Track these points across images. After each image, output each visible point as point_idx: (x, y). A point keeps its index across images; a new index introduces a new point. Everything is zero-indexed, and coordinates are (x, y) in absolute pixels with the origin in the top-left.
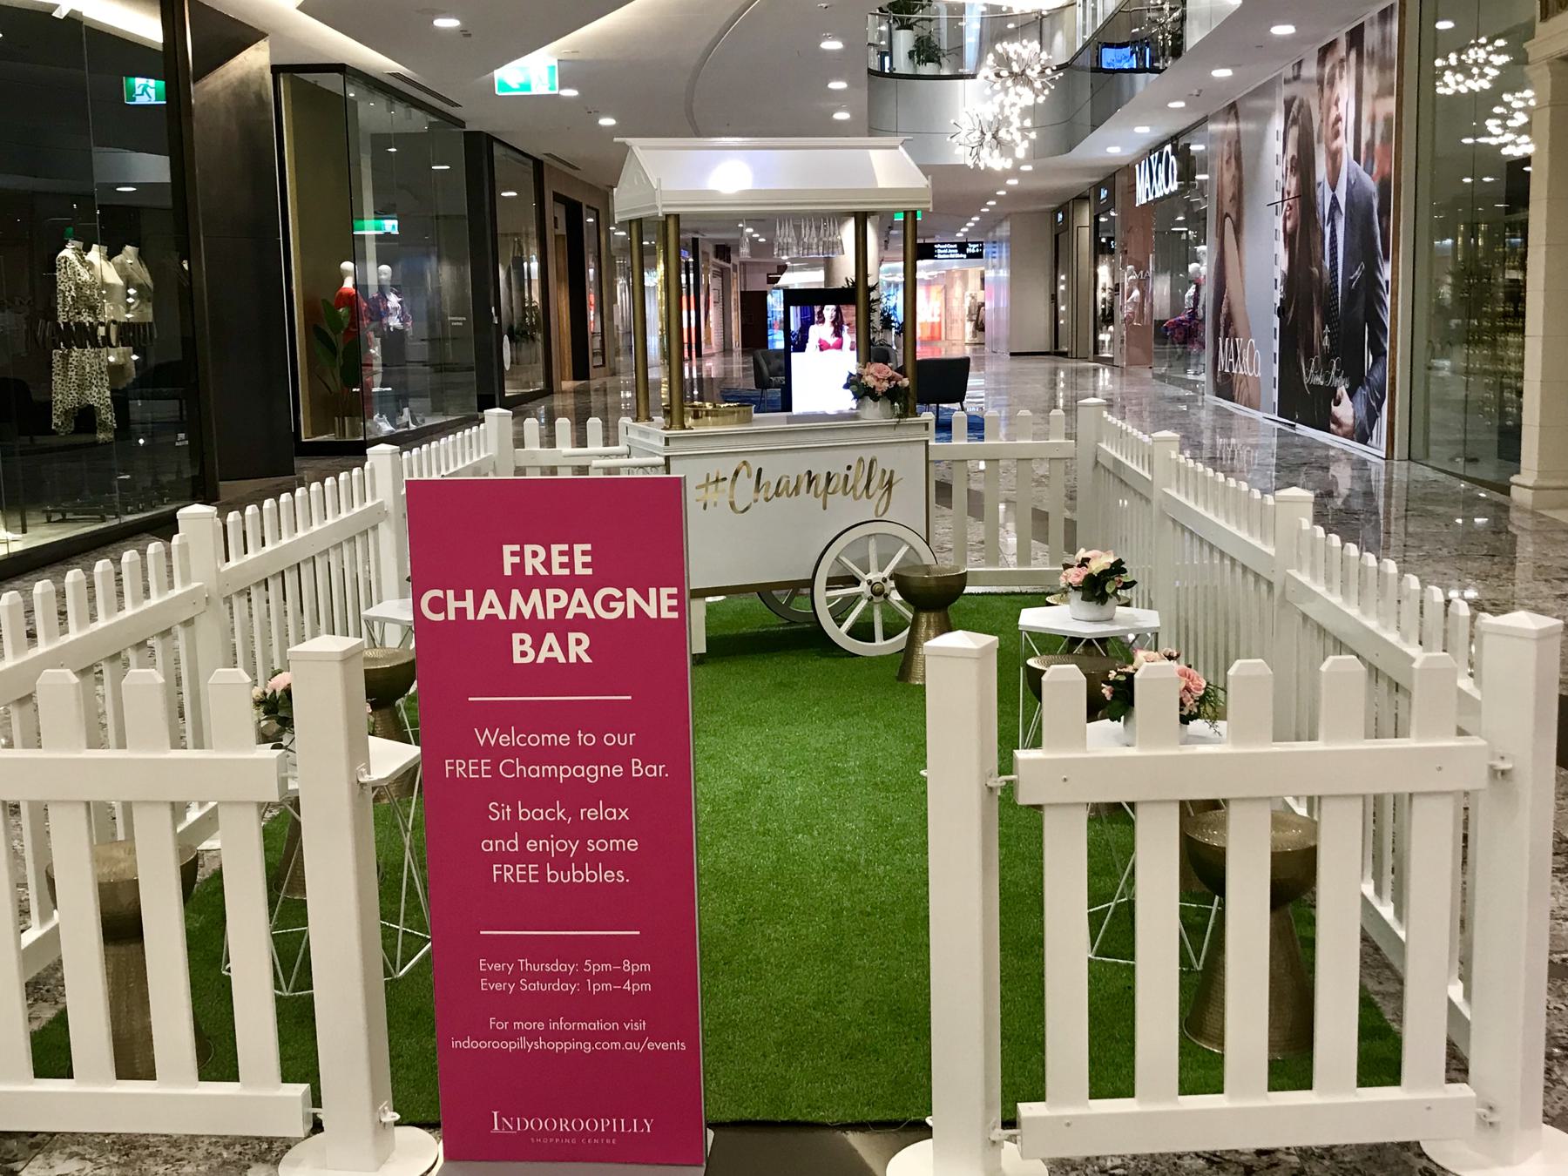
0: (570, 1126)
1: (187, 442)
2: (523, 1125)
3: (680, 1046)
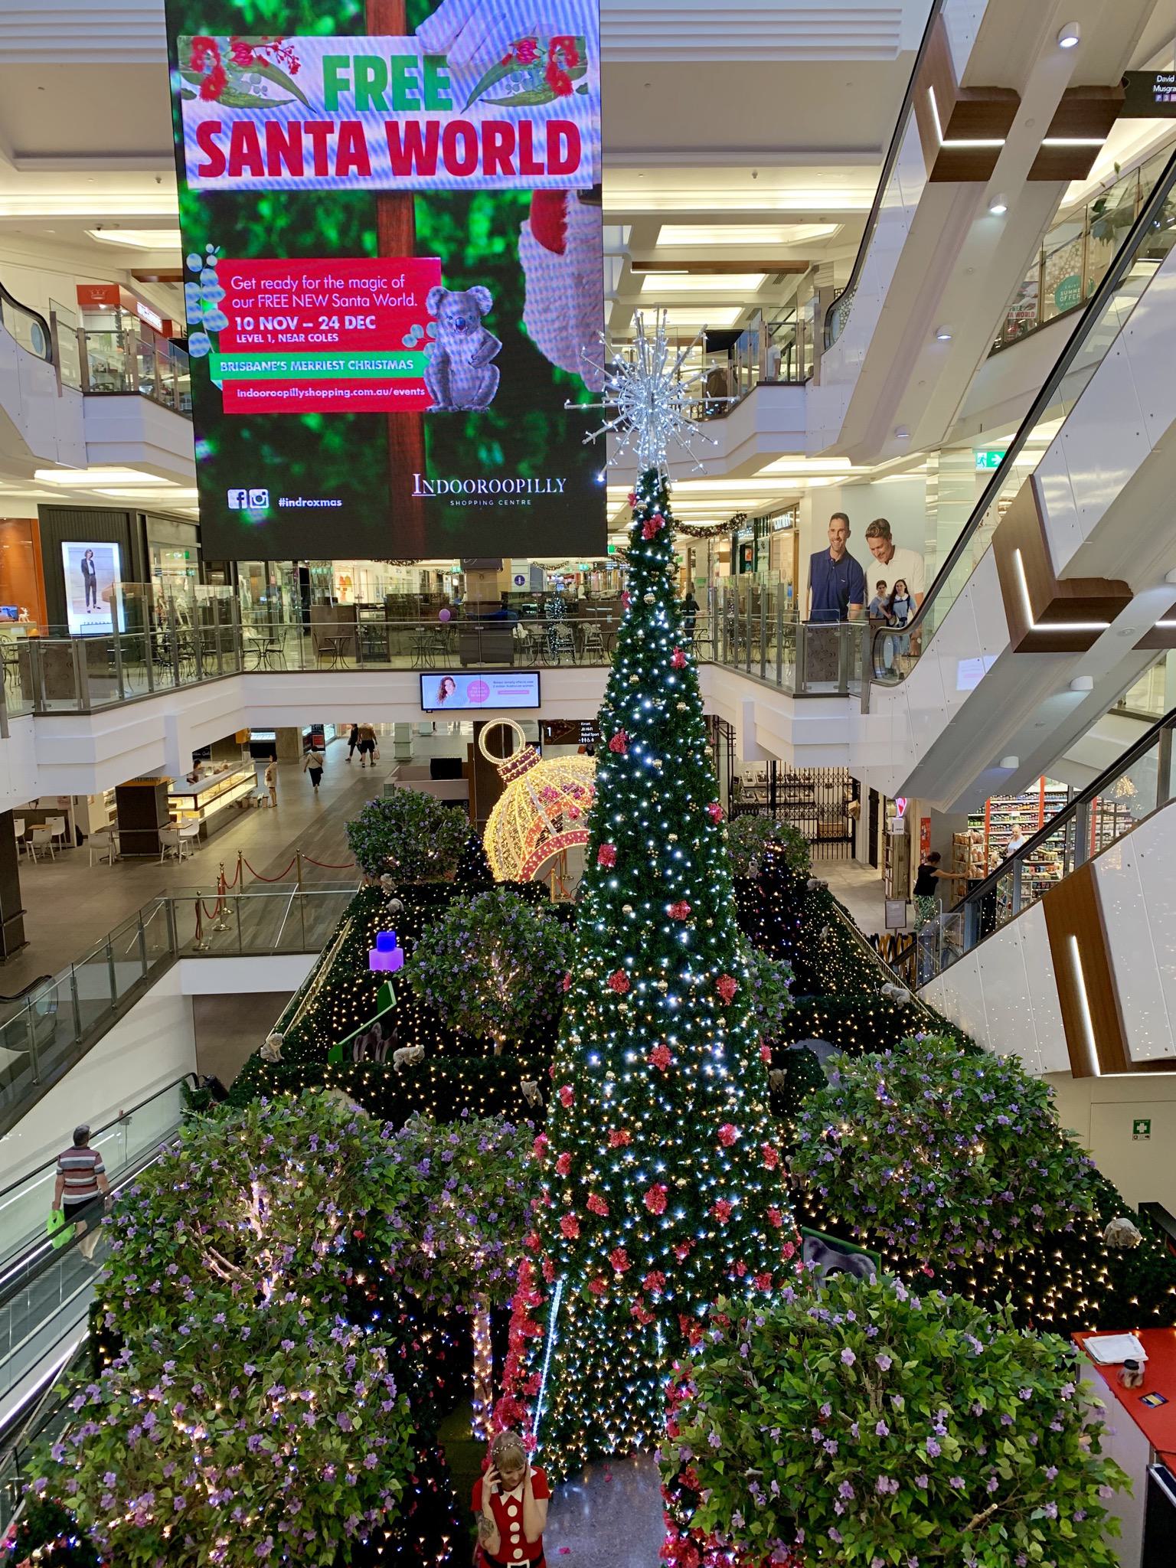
0: (487, 487)
1: (527, 1562)
2: (443, 486)
3: (282, 502)
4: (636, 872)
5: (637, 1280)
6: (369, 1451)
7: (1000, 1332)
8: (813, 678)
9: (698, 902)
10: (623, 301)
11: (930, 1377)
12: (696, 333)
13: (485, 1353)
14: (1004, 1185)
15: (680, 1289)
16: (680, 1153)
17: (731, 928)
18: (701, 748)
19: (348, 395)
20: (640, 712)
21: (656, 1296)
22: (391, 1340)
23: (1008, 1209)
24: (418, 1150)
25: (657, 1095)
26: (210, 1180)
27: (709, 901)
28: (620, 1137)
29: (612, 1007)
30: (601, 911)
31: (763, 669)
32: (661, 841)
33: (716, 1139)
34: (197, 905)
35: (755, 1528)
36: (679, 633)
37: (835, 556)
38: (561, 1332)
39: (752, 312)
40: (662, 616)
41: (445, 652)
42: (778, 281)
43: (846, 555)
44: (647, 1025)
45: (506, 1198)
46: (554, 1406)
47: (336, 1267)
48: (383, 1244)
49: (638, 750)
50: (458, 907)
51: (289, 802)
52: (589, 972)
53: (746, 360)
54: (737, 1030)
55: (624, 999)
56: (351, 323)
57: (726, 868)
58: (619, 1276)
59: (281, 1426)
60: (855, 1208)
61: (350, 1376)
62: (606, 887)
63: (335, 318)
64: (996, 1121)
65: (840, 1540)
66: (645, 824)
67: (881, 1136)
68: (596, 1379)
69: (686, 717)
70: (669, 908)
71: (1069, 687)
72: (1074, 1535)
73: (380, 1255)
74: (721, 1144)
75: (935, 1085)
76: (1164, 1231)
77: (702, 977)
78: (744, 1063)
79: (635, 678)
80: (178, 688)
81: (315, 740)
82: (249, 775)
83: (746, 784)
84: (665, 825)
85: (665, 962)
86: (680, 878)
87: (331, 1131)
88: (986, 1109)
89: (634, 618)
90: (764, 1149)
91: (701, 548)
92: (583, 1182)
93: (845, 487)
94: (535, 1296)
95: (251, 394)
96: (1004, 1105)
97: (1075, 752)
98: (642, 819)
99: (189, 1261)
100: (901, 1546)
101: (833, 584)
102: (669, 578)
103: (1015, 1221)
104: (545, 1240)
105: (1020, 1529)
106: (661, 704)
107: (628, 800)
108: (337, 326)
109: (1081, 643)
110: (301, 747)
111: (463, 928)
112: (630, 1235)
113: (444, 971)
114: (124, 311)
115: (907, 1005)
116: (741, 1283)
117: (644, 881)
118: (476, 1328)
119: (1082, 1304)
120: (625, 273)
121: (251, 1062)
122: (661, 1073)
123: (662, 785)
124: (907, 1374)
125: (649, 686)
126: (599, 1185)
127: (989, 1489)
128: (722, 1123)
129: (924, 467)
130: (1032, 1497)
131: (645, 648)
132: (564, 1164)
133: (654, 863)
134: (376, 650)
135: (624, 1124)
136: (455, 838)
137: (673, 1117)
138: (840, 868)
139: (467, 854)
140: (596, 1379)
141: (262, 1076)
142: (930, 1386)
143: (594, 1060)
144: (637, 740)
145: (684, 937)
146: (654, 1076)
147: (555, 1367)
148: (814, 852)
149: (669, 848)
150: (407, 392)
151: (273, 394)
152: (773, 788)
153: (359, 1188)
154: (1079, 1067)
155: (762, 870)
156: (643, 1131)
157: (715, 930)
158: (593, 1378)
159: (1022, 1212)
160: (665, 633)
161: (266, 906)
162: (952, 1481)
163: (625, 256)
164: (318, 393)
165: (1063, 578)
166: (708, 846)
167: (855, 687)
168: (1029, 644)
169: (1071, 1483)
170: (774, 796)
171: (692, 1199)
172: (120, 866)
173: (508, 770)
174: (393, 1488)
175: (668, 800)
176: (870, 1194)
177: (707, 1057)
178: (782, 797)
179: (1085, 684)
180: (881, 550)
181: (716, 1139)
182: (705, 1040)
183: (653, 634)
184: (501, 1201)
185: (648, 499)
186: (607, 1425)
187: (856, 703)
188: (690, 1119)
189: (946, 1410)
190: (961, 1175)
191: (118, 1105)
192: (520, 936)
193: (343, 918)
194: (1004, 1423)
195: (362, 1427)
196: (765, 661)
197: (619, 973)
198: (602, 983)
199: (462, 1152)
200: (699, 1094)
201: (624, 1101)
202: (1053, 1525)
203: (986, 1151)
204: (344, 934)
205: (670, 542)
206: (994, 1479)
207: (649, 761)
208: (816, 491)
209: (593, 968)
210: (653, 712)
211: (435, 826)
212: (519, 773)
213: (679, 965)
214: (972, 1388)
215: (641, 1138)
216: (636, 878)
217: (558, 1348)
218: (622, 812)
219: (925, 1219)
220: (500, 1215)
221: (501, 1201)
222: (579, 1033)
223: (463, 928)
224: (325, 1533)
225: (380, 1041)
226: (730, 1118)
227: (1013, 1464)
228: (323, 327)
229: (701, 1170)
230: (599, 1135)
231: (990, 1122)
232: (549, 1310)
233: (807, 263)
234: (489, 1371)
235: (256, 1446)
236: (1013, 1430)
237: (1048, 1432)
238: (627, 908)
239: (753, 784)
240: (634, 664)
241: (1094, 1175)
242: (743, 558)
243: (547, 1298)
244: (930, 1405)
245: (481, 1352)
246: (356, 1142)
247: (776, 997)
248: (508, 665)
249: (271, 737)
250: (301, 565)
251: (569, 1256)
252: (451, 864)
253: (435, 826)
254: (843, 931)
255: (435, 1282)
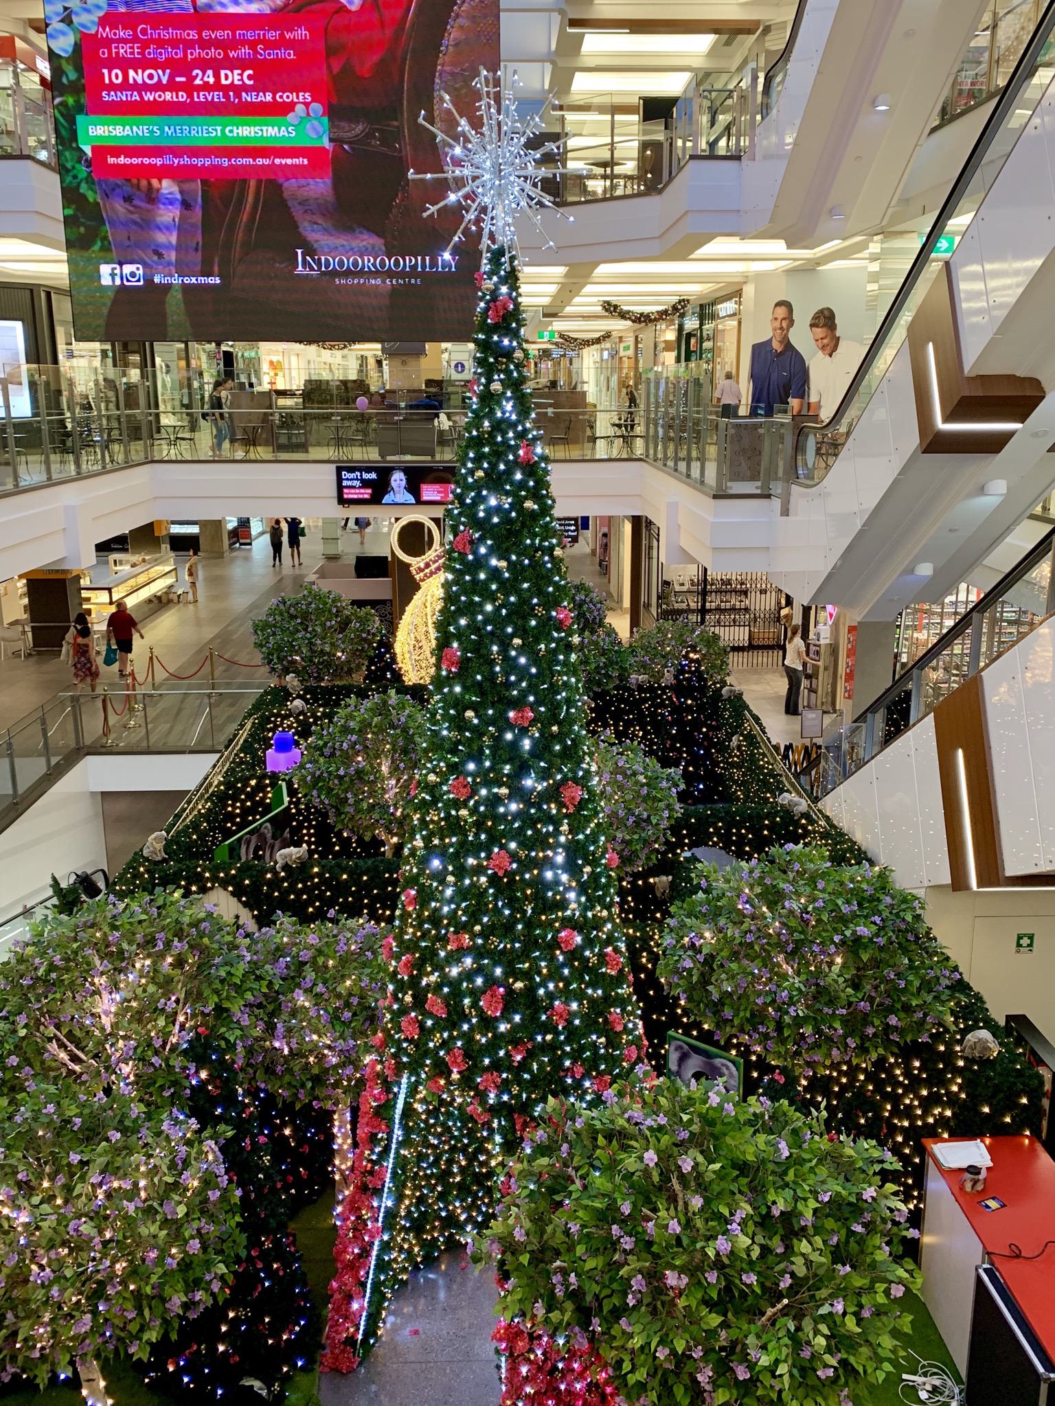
4: (479, 677)
5: (473, 1080)
6: (192, 1237)
7: (817, 1138)
8: (737, 477)
9: (542, 709)
10: (561, 63)
11: (735, 1179)
12: (635, 100)
13: (345, 1147)
14: (860, 995)
15: (515, 1090)
16: (518, 957)
17: (578, 735)
18: (551, 549)
19: (226, 164)
20: (485, 511)
21: (492, 1095)
22: (230, 1134)
23: (866, 1020)
24: (277, 949)
25: (496, 899)
26: (54, 975)
27: (554, 708)
28: (458, 940)
29: (453, 813)
30: (446, 716)
31: (676, 464)
32: (505, 646)
33: (555, 944)
34: (104, 701)
35: (555, 1316)
36: (528, 425)
37: (777, 346)
38: (407, 1130)
39: (702, 78)
40: (509, 406)
41: (365, 443)
42: (728, 43)
43: (788, 346)
44: (489, 832)
45: (361, 998)
46: (400, 1198)
47: (177, 1062)
48: (227, 1041)
49: (483, 550)
50: (349, 709)
51: (214, 598)
52: (432, 778)
53: (680, 132)
54: (581, 837)
55: (465, 804)
56: (227, 77)
57: (575, 674)
58: (455, 1076)
59: (102, 1213)
60: (714, 1014)
61: (180, 1167)
62: (451, 691)
63: (210, 72)
64: (854, 932)
65: (629, 1330)
66: (489, 628)
67: (740, 944)
68: (453, 1175)
69: (534, 516)
70: (511, 714)
71: (981, 490)
72: (860, 1330)
73: (224, 1052)
74: (560, 948)
75: (798, 895)
76: (1027, 1043)
77: (545, 784)
78: (588, 869)
79: (480, 474)
80: (80, 476)
81: (241, 533)
82: (168, 569)
83: (678, 588)
84: (510, 630)
85: (507, 768)
86: (524, 684)
87: (181, 929)
88: (844, 920)
89: (481, 409)
90: (606, 954)
91: (647, 335)
92: (424, 983)
93: (790, 272)
94: (380, 1093)
95: (122, 160)
96: (866, 917)
97: (991, 560)
98: (486, 622)
99: (31, 1053)
100: (687, 1336)
101: (774, 377)
102: (517, 366)
103: (870, 1031)
104: (388, 1039)
105: (807, 1324)
106: (507, 502)
107: (472, 602)
108: (212, 80)
109: (994, 444)
110: (226, 542)
111: (352, 732)
112: (468, 1038)
113: (330, 773)
114: (22, 66)
115: (806, 815)
116: (578, 1084)
117: (487, 685)
118: (336, 1123)
119: (936, 1112)
120: (562, 31)
121: (134, 860)
122: (501, 879)
123: (508, 587)
124: (709, 1176)
125: (495, 481)
126: (439, 986)
127: (782, 1285)
128: (563, 927)
129: (865, 254)
130: (823, 1293)
131: (491, 441)
132: (406, 965)
133: (498, 669)
134: (294, 440)
135: (462, 928)
136: (365, 640)
137: (512, 921)
138: (769, 677)
139: (376, 656)
140: (453, 1175)
141: (143, 874)
142: (735, 1188)
143: (436, 863)
144: (482, 540)
145: (527, 744)
146: (494, 880)
147: (401, 1162)
148: (734, 659)
149: (513, 653)
150: (289, 161)
151: (146, 161)
152: (704, 593)
153: (205, 985)
154: (958, 882)
155: (676, 677)
156: (481, 934)
157: (560, 737)
158: (448, 1173)
159: (877, 1022)
160: (513, 425)
161: (182, 701)
162: (744, 1277)
163: (562, 12)
164: (195, 161)
165: (973, 374)
166: (555, 652)
167: (777, 488)
168: (936, 444)
169: (859, 1282)
170: (704, 601)
171: (529, 1002)
172: (33, 660)
173: (421, 570)
174: (219, 1272)
175: (513, 604)
176: (728, 1001)
177: (548, 863)
178: (713, 602)
179: (999, 487)
180: (825, 341)
181: (555, 944)
182: (545, 846)
183: (500, 426)
184: (355, 1001)
185: (495, 279)
186: (463, 1217)
187: (776, 503)
188: (529, 924)
189: (745, 1209)
190: (817, 985)
191: (23, 898)
192: (410, 739)
193: (245, 718)
194: (803, 1223)
195: (187, 1214)
196: (689, 460)
197: (461, 778)
198: (445, 788)
199: (320, 952)
200: (538, 898)
201: (464, 905)
202: (838, 1320)
203: (844, 966)
204: (244, 735)
205: (520, 325)
206: (787, 1276)
207: (494, 562)
208: (759, 277)
209: (436, 773)
210: (498, 509)
211: (344, 626)
212: (432, 574)
213: (522, 769)
214: (772, 1191)
215: (480, 941)
216: (480, 684)
217: (401, 1144)
218: (465, 615)
219: (779, 1027)
220: (355, 1014)
221: (355, 1001)
222: (423, 838)
223: (352, 732)
224: (147, 1313)
225: (270, 841)
226: (570, 923)
227: (809, 1263)
228: (198, 82)
229: (539, 973)
230: (439, 938)
231: (848, 933)
232: (394, 1106)
233: (758, 23)
234: (349, 1164)
235: (76, 1230)
236: (811, 1231)
237: (851, 1233)
238: (469, 714)
239: (685, 588)
240: (478, 460)
241: (961, 986)
242: (688, 347)
243: (391, 1096)
244: (728, 1205)
245: (340, 1145)
246: (206, 940)
247: (662, 805)
248: (429, 458)
249: (195, 530)
250: (224, 348)
251: (409, 1055)
252: (359, 666)
253: (344, 626)
254: (751, 739)
255: (287, 1078)
